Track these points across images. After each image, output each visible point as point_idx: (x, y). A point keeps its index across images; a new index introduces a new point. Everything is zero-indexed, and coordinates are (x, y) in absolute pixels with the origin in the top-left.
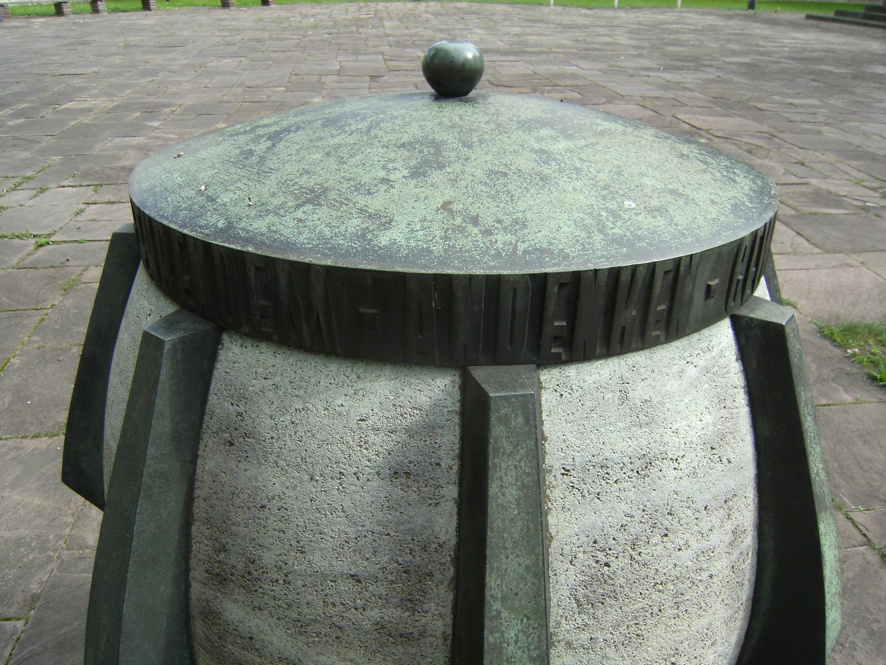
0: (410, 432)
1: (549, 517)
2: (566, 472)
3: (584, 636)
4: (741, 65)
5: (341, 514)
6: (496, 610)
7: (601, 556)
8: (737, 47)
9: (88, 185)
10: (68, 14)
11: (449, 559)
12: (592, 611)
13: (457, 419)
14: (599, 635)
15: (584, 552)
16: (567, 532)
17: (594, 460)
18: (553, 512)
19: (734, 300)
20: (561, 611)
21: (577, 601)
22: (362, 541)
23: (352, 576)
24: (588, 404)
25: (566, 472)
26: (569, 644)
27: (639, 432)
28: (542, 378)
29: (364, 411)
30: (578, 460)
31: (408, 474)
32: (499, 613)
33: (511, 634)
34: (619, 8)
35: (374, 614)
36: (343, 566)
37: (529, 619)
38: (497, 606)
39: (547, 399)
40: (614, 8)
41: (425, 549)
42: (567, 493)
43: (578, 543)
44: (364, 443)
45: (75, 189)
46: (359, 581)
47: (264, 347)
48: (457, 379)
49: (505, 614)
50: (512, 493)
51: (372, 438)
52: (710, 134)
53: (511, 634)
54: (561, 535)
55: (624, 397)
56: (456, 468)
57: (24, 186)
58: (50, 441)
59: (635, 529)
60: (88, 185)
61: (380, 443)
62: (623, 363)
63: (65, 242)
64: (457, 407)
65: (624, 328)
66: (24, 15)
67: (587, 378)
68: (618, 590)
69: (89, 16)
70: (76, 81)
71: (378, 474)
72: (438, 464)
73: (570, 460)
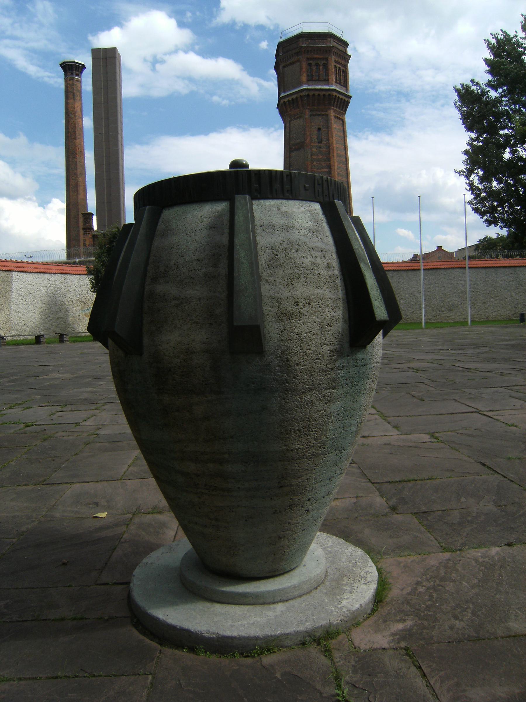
0: (215, 217)
1: (257, 238)
2: (261, 226)
3: (272, 279)
4: (506, 345)
5: (195, 242)
6: (238, 248)
7: (274, 251)
8: (507, 338)
9: (58, 405)
10: (43, 343)
11: (226, 250)
12: (273, 270)
13: (228, 212)
14: (276, 279)
15: (269, 250)
16: (263, 243)
17: (270, 224)
18: (258, 236)
19: (318, 196)
20: (263, 268)
21: (268, 265)
22: (201, 248)
23: (197, 259)
24: (267, 209)
25: (261, 226)
26: (267, 281)
27: (285, 219)
28: (253, 202)
29: (202, 214)
30: (265, 223)
31: (214, 228)
32: (238, 250)
33: (242, 255)
34: (426, 328)
35: (204, 271)
36: (194, 257)
37: (247, 251)
38: (238, 247)
39: (255, 207)
40: (422, 329)
41: (219, 247)
42: (262, 232)
43: (267, 246)
44: (202, 222)
45: (48, 407)
46: (199, 261)
47: (175, 207)
48: (229, 203)
49: (240, 250)
50: (241, 218)
51: (204, 219)
52: (476, 370)
53: (242, 255)
54: (261, 243)
55: (279, 209)
56: (228, 225)
57: (16, 407)
58: (33, 487)
59: (286, 246)
60: (58, 405)
61: (206, 221)
62: (278, 201)
63: (43, 424)
64: (229, 209)
65: (276, 190)
66: (15, 344)
67: (267, 203)
68: (282, 264)
69: (57, 345)
70: (50, 368)
71: (206, 228)
72: (223, 224)
73: (262, 223)
